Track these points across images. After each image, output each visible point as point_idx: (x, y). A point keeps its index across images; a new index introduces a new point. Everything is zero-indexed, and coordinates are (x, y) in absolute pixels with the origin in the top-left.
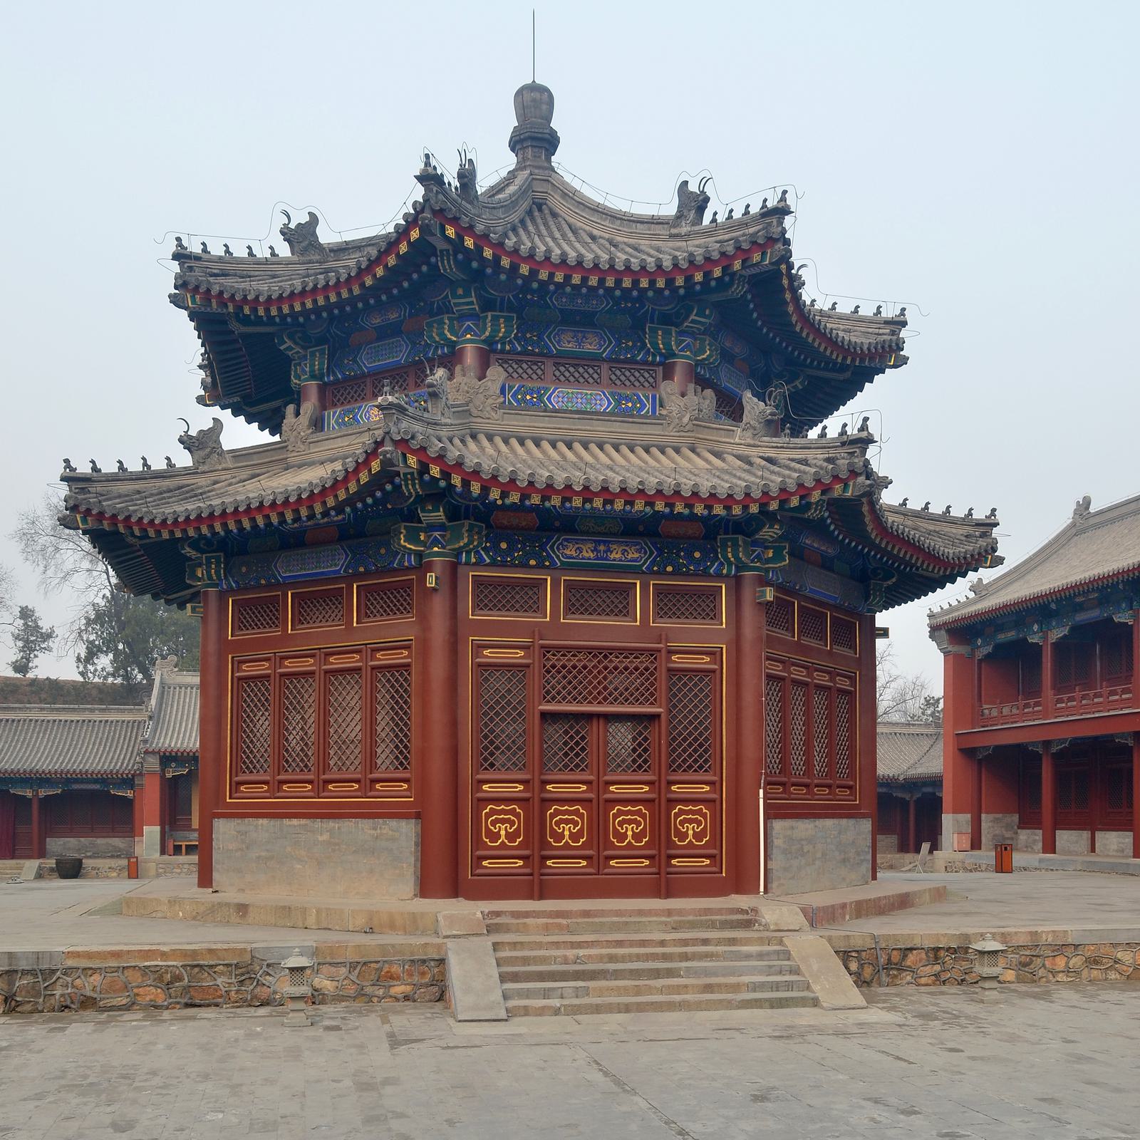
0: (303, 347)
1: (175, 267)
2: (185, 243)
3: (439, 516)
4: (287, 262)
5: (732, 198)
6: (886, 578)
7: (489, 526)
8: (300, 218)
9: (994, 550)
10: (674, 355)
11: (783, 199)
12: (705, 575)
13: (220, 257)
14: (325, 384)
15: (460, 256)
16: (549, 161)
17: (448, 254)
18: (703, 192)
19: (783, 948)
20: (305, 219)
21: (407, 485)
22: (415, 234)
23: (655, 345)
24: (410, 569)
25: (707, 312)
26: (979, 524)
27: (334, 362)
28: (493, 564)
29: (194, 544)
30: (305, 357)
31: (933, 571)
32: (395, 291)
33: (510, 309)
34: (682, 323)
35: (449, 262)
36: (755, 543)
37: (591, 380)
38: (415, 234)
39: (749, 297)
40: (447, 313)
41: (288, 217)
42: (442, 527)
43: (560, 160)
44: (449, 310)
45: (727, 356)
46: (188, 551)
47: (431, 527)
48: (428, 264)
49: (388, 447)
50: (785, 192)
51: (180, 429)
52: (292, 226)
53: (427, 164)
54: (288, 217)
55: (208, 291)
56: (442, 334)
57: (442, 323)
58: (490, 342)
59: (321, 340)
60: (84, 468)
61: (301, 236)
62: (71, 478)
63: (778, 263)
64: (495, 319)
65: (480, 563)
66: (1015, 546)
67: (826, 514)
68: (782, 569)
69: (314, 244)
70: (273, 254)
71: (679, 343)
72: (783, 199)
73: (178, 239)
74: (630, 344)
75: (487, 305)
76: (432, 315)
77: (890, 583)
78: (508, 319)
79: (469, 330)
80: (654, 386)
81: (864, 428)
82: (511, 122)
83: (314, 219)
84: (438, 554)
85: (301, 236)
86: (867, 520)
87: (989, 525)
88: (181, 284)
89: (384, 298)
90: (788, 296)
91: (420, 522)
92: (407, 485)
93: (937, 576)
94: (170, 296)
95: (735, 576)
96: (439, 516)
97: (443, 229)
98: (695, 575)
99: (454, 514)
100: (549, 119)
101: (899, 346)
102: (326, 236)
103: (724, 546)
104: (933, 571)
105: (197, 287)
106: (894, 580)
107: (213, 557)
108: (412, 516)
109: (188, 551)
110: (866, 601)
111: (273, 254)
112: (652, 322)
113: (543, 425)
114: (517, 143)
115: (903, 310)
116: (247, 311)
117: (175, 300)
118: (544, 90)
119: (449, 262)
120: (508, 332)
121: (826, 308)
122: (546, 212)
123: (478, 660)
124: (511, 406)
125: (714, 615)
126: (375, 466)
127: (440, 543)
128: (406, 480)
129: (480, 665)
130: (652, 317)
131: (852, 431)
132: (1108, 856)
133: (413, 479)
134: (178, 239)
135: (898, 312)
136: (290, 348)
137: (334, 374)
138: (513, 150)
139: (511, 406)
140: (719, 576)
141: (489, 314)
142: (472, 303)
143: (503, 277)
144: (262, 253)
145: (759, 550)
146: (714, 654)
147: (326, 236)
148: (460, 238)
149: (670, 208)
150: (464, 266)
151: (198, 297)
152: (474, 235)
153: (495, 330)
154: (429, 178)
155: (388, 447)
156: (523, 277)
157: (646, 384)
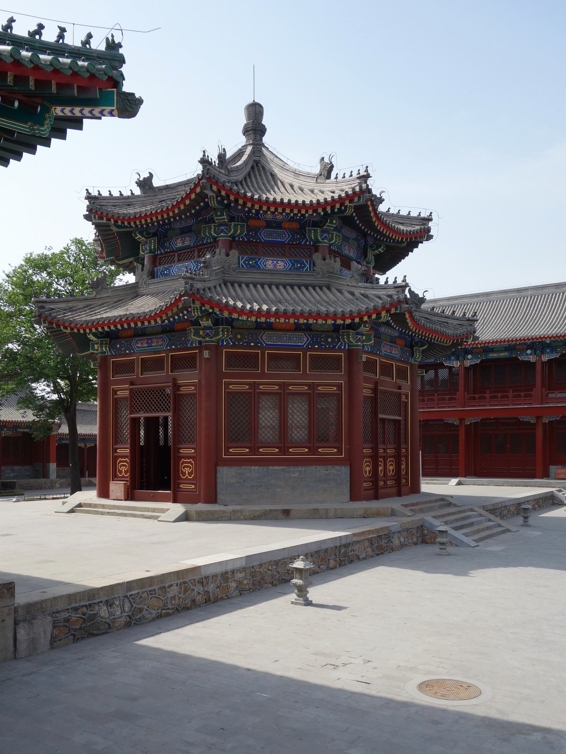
0: (145, 238)
1: (87, 202)
2: (90, 191)
3: (209, 323)
4: (138, 196)
5: (346, 168)
6: (421, 346)
7: (232, 327)
9: (475, 332)
10: (319, 242)
11: (367, 171)
12: (333, 349)
13: (107, 197)
14: (156, 255)
15: (219, 198)
16: (261, 140)
17: (213, 198)
18: (331, 163)
19: (445, 503)
21: (194, 312)
22: (198, 190)
23: (310, 237)
24: (195, 348)
25: (334, 222)
26: (424, 219)
27: (161, 244)
29: (95, 335)
30: (146, 243)
31: (446, 343)
32: (188, 214)
33: (243, 221)
34: (323, 227)
35: (214, 201)
36: (358, 334)
37: (280, 254)
38: (198, 190)
39: (354, 214)
40: (213, 223)
41: (139, 175)
42: (210, 328)
44: (214, 222)
45: (346, 239)
46: (91, 337)
47: (205, 328)
48: (204, 202)
50: (367, 167)
52: (141, 179)
53: (204, 155)
54: (139, 175)
55: (102, 213)
56: (210, 233)
57: (210, 228)
58: (233, 237)
59: (155, 235)
60: (95, 193)
61: (145, 184)
62: (89, 197)
63: (367, 201)
64: (236, 226)
67: (390, 319)
68: (371, 345)
70: (132, 194)
71: (321, 236)
72: (367, 171)
73: (87, 190)
74: (298, 236)
75: (232, 219)
76: (206, 223)
77: (424, 348)
78: (242, 226)
80: (310, 256)
81: (404, 280)
83: (151, 175)
84: (222, 236)
85: (145, 184)
86: (408, 321)
87: (472, 321)
88: (90, 209)
89: (183, 217)
90: (372, 214)
91: (200, 325)
92: (194, 312)
93: (447, 345)
94: (84, 215)
95: (348, 349)
96: (209, 323)
97: (211, 187)
98: (330, 350)
99: (217, 322)
101: (429, 230)
102: (156, 183)
103: (343, 335)
104: (446, 343)
105: (96, 211)
106: (426, 347)
107: (104, 340)
108: (196, 323)
109: (91, 337)
110: (412, 357)
111: (132, 194)
112: (309, 227)
113: (257, 277)
114: (246, 132)
115: (431, 213)
116: (120, 223)
117: (87, 217)
118: (260, 106)
119: (214, 201)
120: (242, 232)
121: (395, 213)
122: (260, 167)
123: (227, 390)
125: (339, 368)
127: (210, 335)
128: (194, 310)
129: (228, 393)
130: (309, 223)
131: (399, 281)
132: (168, 609)
133: (197, 309)
134: (87, 190)
135: (429, 214)
136: (139, 238)
137: (160, 250)
138: (244, 134)
140: (340, 349)
141: (233, 223)
142: (224, 219)
143: (240, 207)
144: (127, 193)
145: (359, 336)
146: (339, 386)
147: (156, 183)
148: (219, 191)
149: (317, 170)
150: (220, 203)
151: (97, 216)
152: (225, 190)
153: (236, 231)
154: (204, 161)
156: (248, 208)
157: (306, 255)
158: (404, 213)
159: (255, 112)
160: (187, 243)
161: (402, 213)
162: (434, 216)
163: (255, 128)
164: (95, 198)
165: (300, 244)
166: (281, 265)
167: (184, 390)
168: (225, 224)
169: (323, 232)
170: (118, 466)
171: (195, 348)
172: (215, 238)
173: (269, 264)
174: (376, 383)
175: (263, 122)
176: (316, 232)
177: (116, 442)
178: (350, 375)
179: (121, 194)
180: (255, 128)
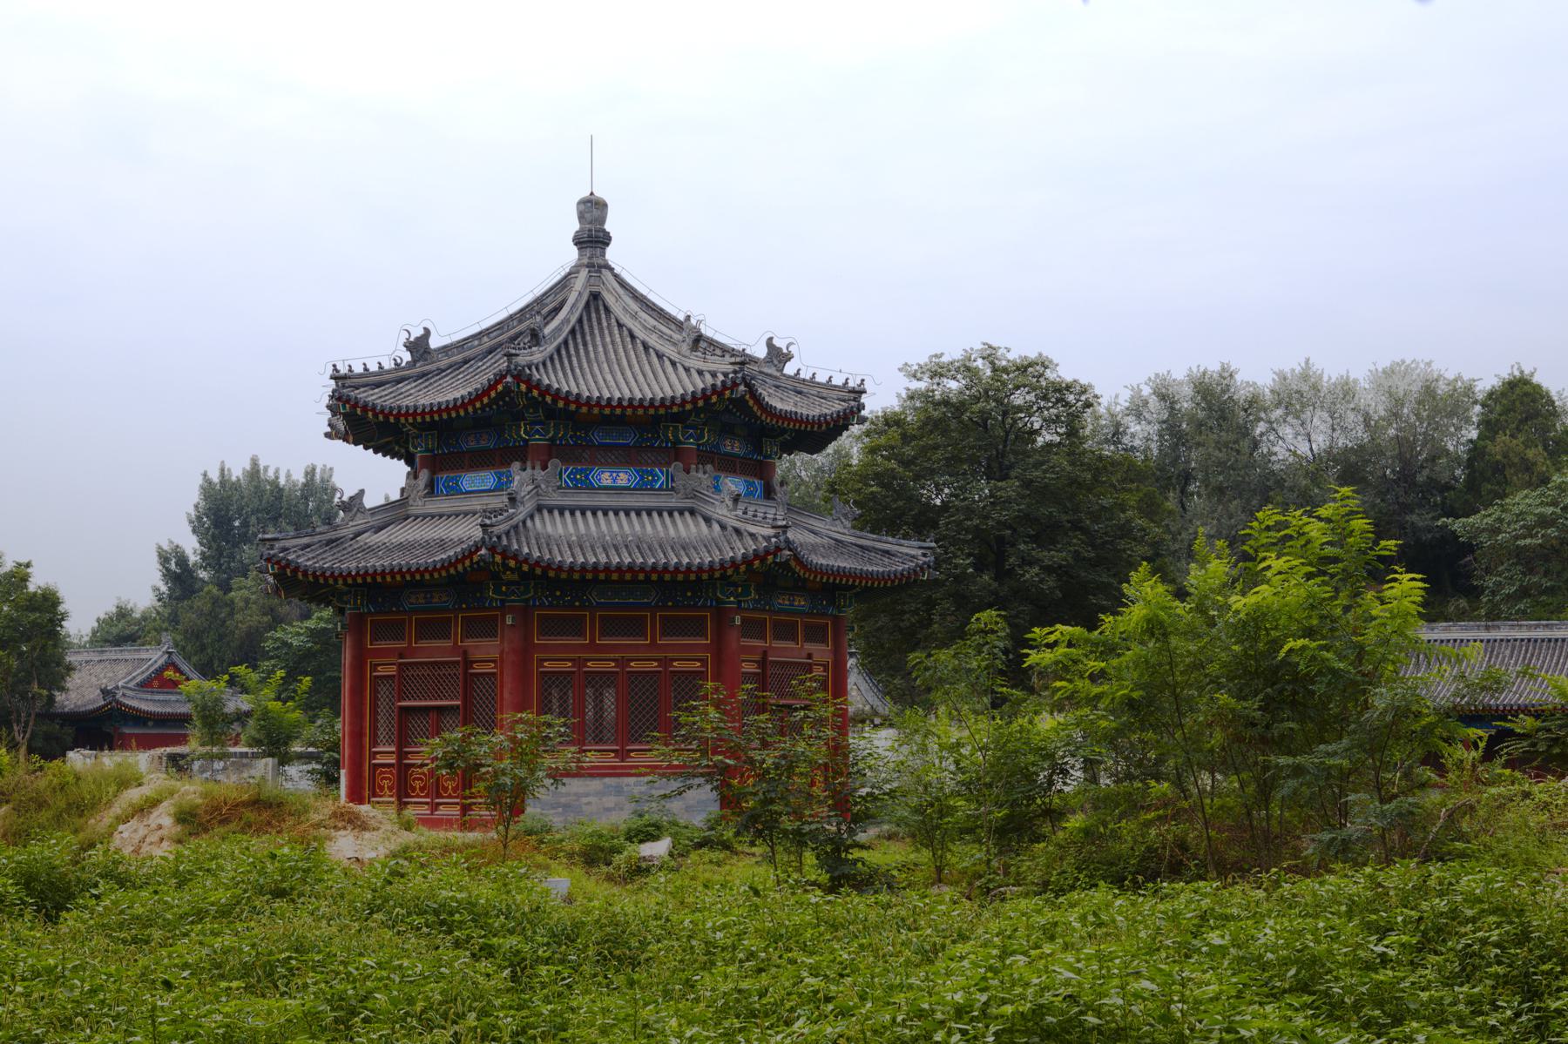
8: (417, 332)
16: (603, 255)
20: (420, 332)
24: (496, 608)
26: (853, 391)
28: (551, 606)
43: (612, 255)
49: (509, 379)
51: (403, 340)
58: (552, 440)
60: (343, 370)
62: (336, 377)
65: (542, 605)
66: (877, 403)
69: (427, 351)
79: (537, 432)
82: (575, 226)
83: (427, 332)
100: (602, 220)
113: (584, 499)
114: (579, 241)
124: (568, 487)
126: (500, 388)
139: (568, 487)
155: (509, 379)
158: (821, 378)
159: (593, 210)
160: (483, 444)
161: (818, 379)
162: (867, 386)
163: (593, 239)
164: (345, 377)
165: (652, 446)
166: (623, 479)
167: (477, 669)
168: (540, 423)
169: (686, 427)
170: (378, 780)
171: (496, 608)
172: (526, 441)
173: (606, 479)
174: (765, 653)
175: (608, 227)
176: (676, 428)
177: (374, 743)
178: (719, 637)
179: (381, 367)
180: (593, 239)
